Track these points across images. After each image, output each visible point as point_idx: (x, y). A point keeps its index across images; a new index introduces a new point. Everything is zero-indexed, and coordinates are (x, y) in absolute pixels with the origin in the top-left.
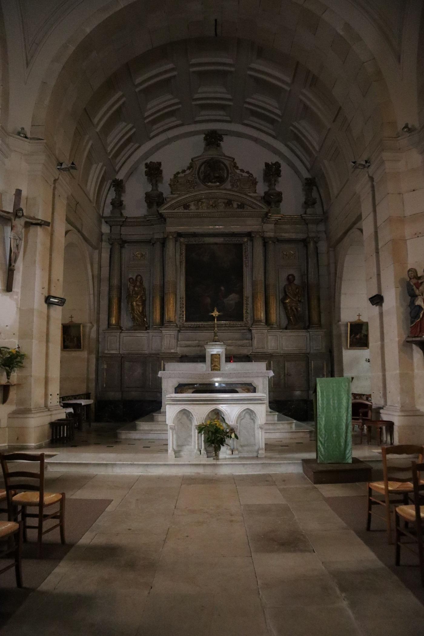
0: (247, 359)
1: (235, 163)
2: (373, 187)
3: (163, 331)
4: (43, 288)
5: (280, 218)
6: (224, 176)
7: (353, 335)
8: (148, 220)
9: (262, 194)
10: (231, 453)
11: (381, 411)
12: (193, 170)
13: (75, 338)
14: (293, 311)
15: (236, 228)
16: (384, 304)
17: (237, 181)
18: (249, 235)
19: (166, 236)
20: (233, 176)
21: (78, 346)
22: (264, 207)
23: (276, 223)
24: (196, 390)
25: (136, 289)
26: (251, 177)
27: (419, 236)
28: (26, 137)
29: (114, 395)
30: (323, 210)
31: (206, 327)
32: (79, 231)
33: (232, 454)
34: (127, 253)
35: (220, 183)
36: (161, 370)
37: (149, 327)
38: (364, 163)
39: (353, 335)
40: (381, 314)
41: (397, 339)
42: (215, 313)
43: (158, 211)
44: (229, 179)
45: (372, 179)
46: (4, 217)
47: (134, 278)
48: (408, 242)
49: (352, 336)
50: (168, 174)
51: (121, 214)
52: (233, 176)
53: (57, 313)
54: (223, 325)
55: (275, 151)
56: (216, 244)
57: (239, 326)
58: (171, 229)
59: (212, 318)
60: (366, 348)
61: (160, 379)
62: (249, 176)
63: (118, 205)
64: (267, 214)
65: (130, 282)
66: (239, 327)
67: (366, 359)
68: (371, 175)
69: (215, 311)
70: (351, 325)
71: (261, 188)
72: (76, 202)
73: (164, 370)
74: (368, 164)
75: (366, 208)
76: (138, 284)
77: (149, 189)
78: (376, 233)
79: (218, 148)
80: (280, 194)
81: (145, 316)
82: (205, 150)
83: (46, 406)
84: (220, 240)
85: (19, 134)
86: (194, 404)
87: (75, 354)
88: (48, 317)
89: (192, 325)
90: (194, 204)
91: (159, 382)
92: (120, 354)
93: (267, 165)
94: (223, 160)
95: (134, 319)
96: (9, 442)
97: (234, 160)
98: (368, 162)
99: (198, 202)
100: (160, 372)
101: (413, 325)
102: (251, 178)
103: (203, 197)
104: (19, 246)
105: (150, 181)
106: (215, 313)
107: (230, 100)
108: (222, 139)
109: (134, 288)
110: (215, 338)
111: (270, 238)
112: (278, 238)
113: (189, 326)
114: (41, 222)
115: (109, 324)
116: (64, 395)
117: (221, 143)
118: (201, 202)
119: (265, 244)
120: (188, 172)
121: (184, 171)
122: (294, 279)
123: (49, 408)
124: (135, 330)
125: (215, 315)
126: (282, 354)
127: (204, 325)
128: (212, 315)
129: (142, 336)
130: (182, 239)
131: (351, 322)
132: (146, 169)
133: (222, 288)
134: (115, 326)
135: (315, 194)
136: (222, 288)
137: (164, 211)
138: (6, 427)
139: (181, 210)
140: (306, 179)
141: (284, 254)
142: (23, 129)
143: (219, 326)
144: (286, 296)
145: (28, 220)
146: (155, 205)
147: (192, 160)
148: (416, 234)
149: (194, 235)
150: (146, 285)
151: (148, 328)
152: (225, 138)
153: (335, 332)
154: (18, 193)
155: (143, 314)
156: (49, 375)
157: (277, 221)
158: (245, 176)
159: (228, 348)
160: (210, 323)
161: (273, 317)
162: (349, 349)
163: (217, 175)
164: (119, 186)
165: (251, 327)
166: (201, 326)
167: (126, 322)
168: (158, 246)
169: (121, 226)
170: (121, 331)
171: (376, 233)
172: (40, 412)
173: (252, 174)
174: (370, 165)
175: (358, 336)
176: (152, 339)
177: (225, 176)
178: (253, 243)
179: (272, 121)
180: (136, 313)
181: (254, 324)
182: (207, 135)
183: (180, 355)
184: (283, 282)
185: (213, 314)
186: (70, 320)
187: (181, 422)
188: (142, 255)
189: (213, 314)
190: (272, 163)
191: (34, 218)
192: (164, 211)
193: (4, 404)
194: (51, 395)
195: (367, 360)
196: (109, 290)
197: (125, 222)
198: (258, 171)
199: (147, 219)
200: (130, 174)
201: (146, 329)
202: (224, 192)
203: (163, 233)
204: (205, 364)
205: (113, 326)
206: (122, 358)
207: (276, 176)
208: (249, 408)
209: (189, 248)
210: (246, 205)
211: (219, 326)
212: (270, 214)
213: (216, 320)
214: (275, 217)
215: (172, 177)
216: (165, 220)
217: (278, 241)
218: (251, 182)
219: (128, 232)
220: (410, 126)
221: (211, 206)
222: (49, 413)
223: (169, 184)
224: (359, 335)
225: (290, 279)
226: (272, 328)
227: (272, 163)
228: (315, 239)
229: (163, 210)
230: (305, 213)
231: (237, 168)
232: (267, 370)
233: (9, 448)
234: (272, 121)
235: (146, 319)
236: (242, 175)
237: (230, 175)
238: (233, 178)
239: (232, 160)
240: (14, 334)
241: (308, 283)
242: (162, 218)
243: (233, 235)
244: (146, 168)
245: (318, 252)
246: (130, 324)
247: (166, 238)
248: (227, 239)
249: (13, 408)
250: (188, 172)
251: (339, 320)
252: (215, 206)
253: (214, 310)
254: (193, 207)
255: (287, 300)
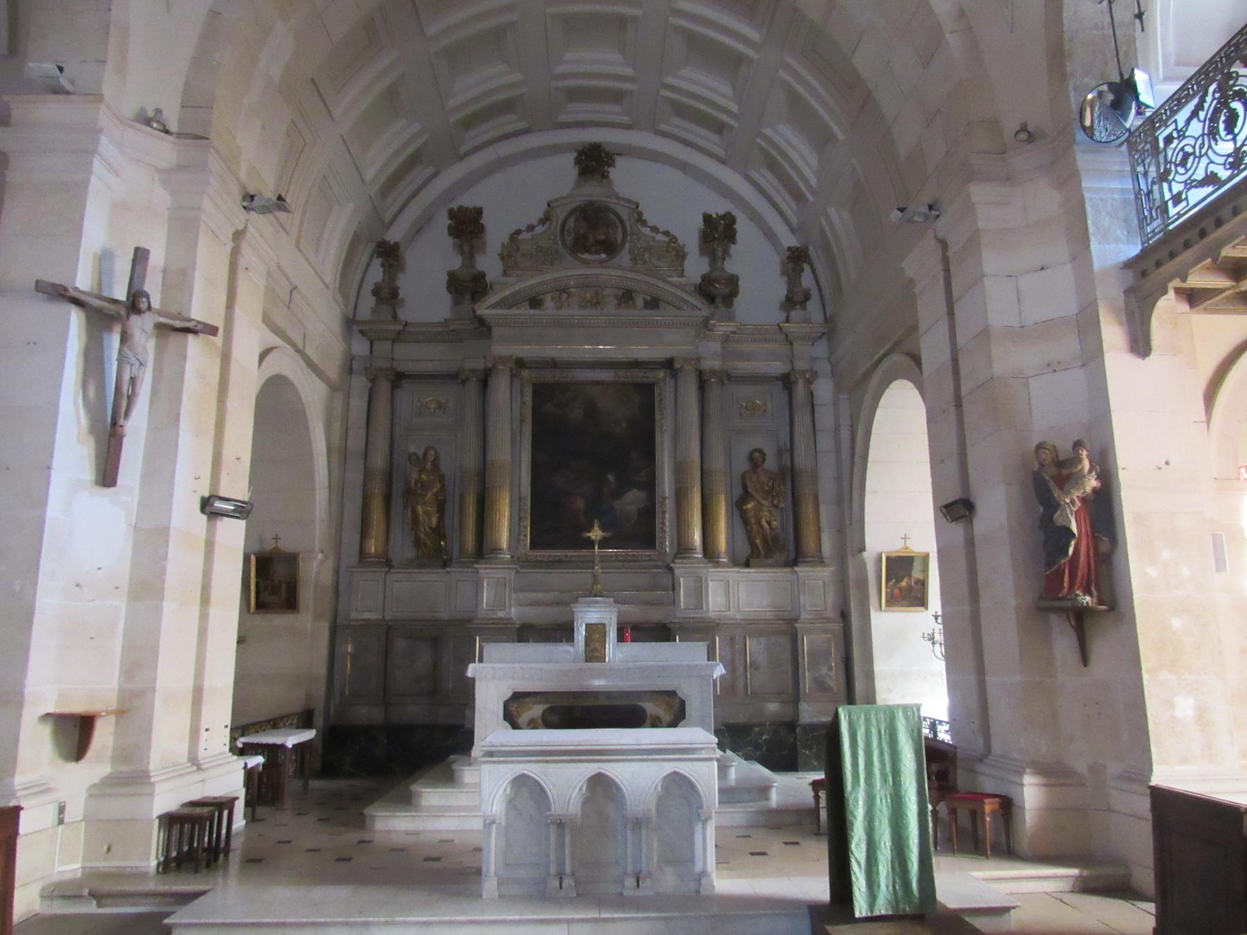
0: (662, 633)
1: (640, 214)
2: (946, 261)
3: (481, 571)
4: (196, 479)
5: (735, 329)
6: (616, 238)
7: (894, 581)
8: (453, 331)
9: (698, 280)
10: (635, 884)
11: (980, 767)
12: (550, 225)
13: (284, 586)
14: (762, 527)
15: (642, 351)
16: (975, 521)
17: (644, 251)
18: (668, 364)
19: (489, 365)
20: (636, 241)
21: (291, 604)
22: (699, 306)
23: (726, 339)
24: (551, 707)
25: (424, 477)
26: (673, 243)
27: (1057, 369)
28: (167, 132)
29: (366, 714)
30: (825, 313)
31: (575, 561)
32: (297, 350)
33: (638, 886)
34: (408, 397)
35: (608, 255)
36: (474, 662)
37: (451, 559)
38: (924, 209)
39: (894, 581)
40: (970, 542)
41: (1012, 602)
42: (596, 534)
43: (474, 312)
44: (627, 245)
45: (944, 245)
46: (105, 311)
47: (421, 454)
48: (1033, 383)
49: (891, 583)
50: (496, 232)
51: (395, 316)
52: (636, 241)
53: (233, 534)
54: (611, 556)
55: (726, 192)
56: (598, 383)
57: (645, 559)
58: (501, 349)
59: (590, 544)
60: (921, 609)
61: (471, 683)
62: (670, 240)
63: (388, 296)
64: (707, 320)
65: (410, 463)
66: (646, 561)
67: (923, 634)
68: (940, 235)
69: (596, 528)
70: (888, 558)
71: (696, 267)
72: (291, 283)
73: (481, 660)
74: (934, 213)
75: (930, 308)
76: (429, 466)
77: (456, 263)
78: (955, 361)
79: (605, 180)
80: (733, 281)
81: (443, 537)
82: (578, 185)
83: (193, 760)
84: (605, 375)
85: (148, 122)
86: (547, 762)
87: (281, 620)
88: (210, 545)
89: (544, 556)
90: (553, 298)
91: (468, 688)
92: (385, 620)
93: (707, 218)
94: (613, 206)
95: (418, 543)
96: (84, 860)
97: (637, 207)
98: (934, 207)
99: (561, 293)
100: (471, 666)
101: (1052, 570)
102: (673, 245)
103: (572, 283)
104: (138, 382)
105: (460, 249)
106: (596, 534)
107: (632, 80)
108: (613, 161)
109: (420, 475)
110: (595, 587)
111: (713, 372)
112: (730, 371)
113: (539, 559)
114: (196, 326)
115: (362, 553)
116: (241, 722)
117: (611, 169)
118: (567, 293)
119: (702, 385)
120: (539, 229)
121: (531, 228)
122: (764, 460)
123: (201, 762)
124: (421, 566)
125: (596, 536)
126: (739, 622)
127: (571, 556)
128: (589, 537)
129: (432, 579)
130: (525, 373)
131: (887, 552)
132: (449, 222)
133: (611, 477)
134: (375, 557)
135: (807, 280)
136: (611, 477)
137: (489, 312)
138: (82, 821)
139: (525, 311)
140: (790, 249)
141: (742, 406)
142: (158, 111)
143: (605, 560)
144: (746, 496)
145: (162, 320)
146: (468, 296)
147: (549, 205)
148: (1049, 365)
149: (553, 364)
150: (445, 467)
151: (448, 563)
152: (620, 161)
153: (852, 573)
154: (140, 256)
155: (439, 532)
156: (207, 683)
157: (728, 336)
158: (659, 241)
159: (625, 608)
160: (584, 552)
161: (722, 541)
162: (886, 611)
163: (603, 237)
164: (390, 254)
165: (673, 562)
166: (563, 559)
167: (402, 548)
168: (472, 388)
169: (394, 341)
170: (387, 569)
171: (955, 361)
172: (174, 777)
173: (674, 237)
174: (938, 216)
175: (903, 584)
176: (457, 586)
177: (619, 240)
178: (676, 384)
179: (719, 128)
180: (423, 530)
181: (679, 556)
182: (580, 153)
183: (517, 622)
184: (742, 465)
185: (590, 534)
186: (274, 546)
187: (515, 807)
188: (440, 405)
189: (590, 534)
190: (717, 214)
191: (179, 316)
192: (489, 312)
193: (80, 762)
194: (207, 730)
195: (926, 635)
196: (364, 478)
197: (402, 335)
198: (689, 233)
199: (451, 328)
200: (418, 230)
201: (445, 564)
202: (619, 273)
203: (485, 357)
204: (573, 646)
205: (372, 557)
206: (388, 630)
207: (726, 241)
208: (678, 770)
209: (542, 392)
210: (663, 301)
211: (605, 560)
212: (713, 322)
213: (596, 547)
214: (722, 328)
215: (506, 240)
216: (489, 330)
217: (729, 377)
218: (674, 253)
219: (412, 356)
220: (1030, 128)
221: (589, 302)
222: (199, 776)
223: (500, 255)
224: (906, 580)
225: (756, 459)
226: (717, 564)
227: (717, 214)
228: (807, 376)
229: (483, 309)
230: (788, 320)
231: (644, 223)
232: (708, 660)
233: (83, 873)
234: (719, 128)
235: (446, 543)
236: (653, 238)
237: (629, 238)
238: (635, 243)
239: (635, 207)
240: (117, 588)
241: (792, 465)
242: (483, 328)
243: (636, 364)
244: (450, 218)
245: (815, 402)
246: (410, 553)
247: (490, 369)
248: (621, 373)
249: (105, 769)
250: (539, 229)
251: (862, 548)
252: (598, 303)
253: (592, 527)
254: (549, 303)
255: (749, 503)
